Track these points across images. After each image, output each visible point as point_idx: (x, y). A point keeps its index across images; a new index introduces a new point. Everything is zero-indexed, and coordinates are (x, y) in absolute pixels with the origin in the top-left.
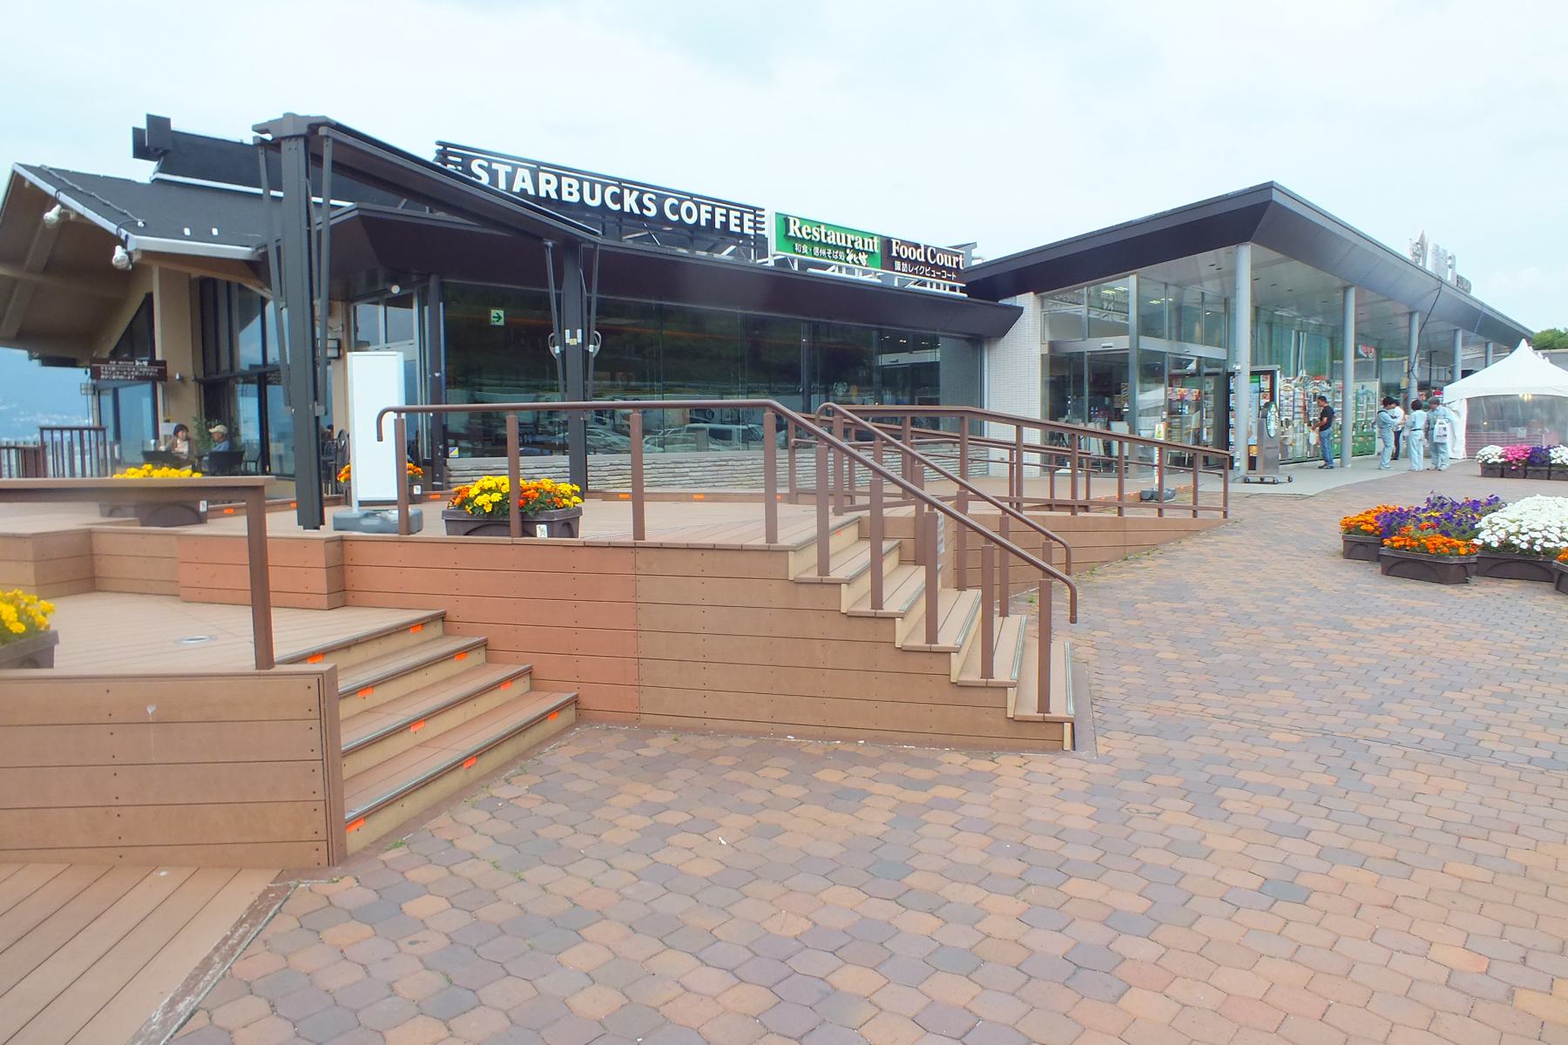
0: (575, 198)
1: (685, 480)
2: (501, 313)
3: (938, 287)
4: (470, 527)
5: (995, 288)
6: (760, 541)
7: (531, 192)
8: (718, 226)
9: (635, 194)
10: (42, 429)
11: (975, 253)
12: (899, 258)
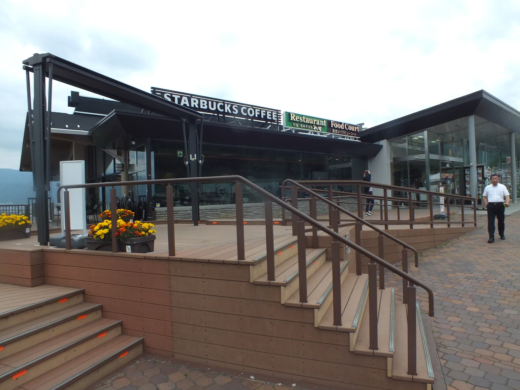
0: (206, 107)
1: (251, 214)
2: (181, 152)
3: (351, 139)
4: (98, 246)
5: (370, 139)
6: (235, 258)
7: (188, 105)
8: (262, 117)
9: (229, 106)
10: (29, 199)
11: (363, 127)
12: (334, 128)
